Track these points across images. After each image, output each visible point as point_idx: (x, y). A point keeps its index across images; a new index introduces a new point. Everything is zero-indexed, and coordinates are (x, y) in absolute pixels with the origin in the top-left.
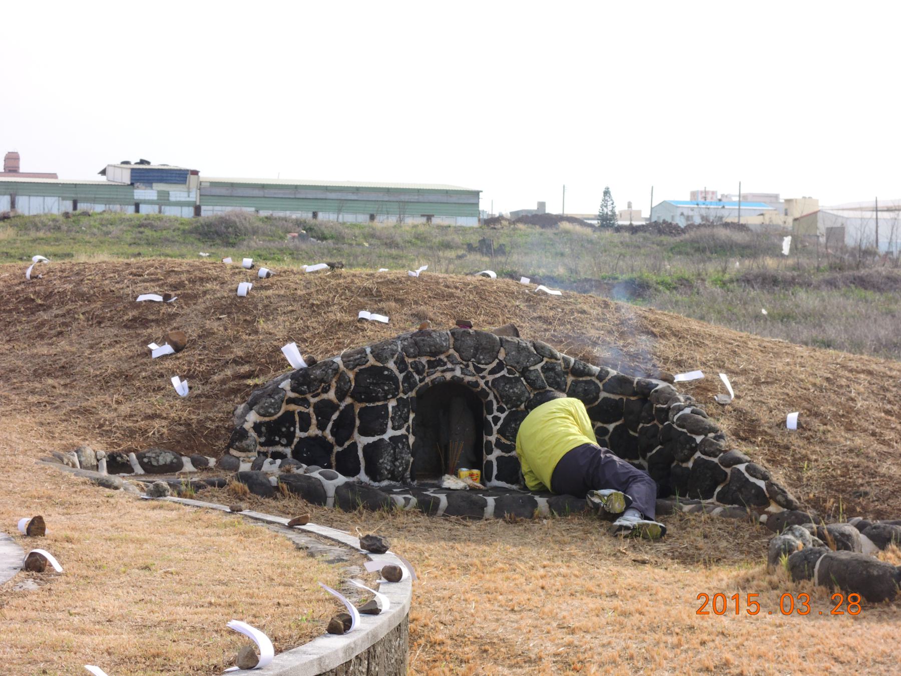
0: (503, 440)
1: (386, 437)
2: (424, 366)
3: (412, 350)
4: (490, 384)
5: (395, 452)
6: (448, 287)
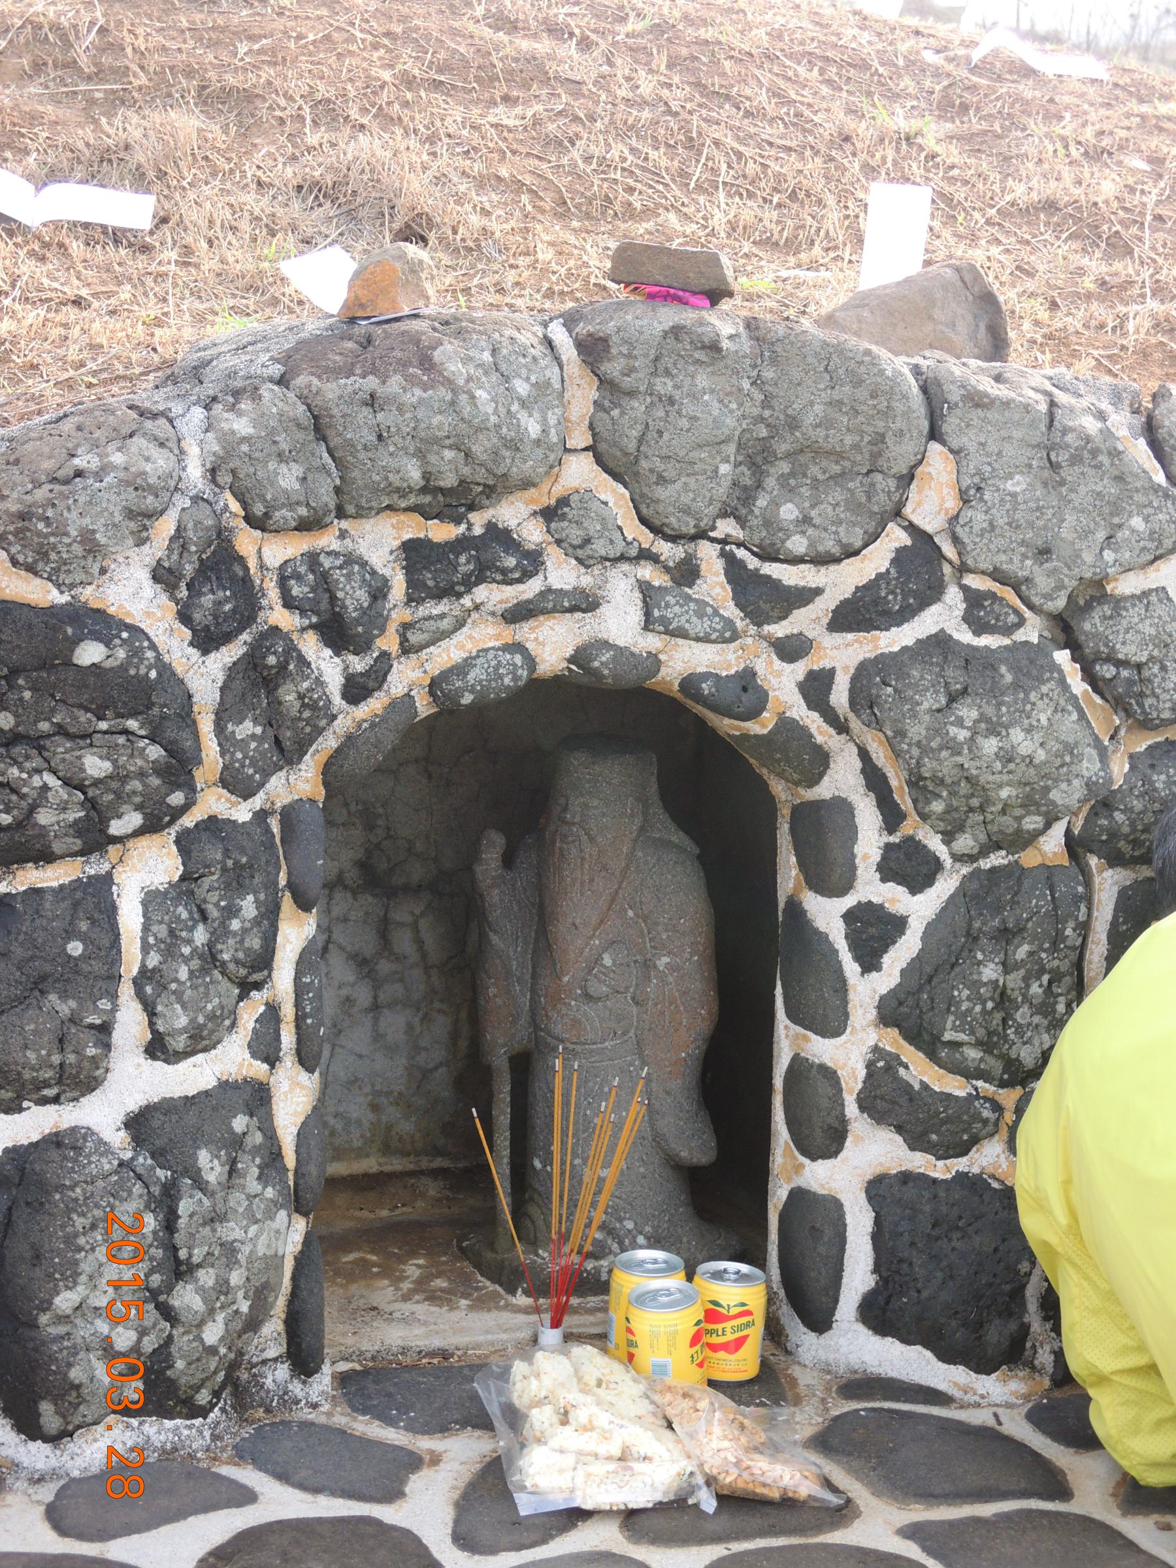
0: (919, 1070)
1: (102, 1114)
2: (379, 592)
3: (288, 478)
4: (839, 697)
5: (170, 1224)
6: (512, 26)
